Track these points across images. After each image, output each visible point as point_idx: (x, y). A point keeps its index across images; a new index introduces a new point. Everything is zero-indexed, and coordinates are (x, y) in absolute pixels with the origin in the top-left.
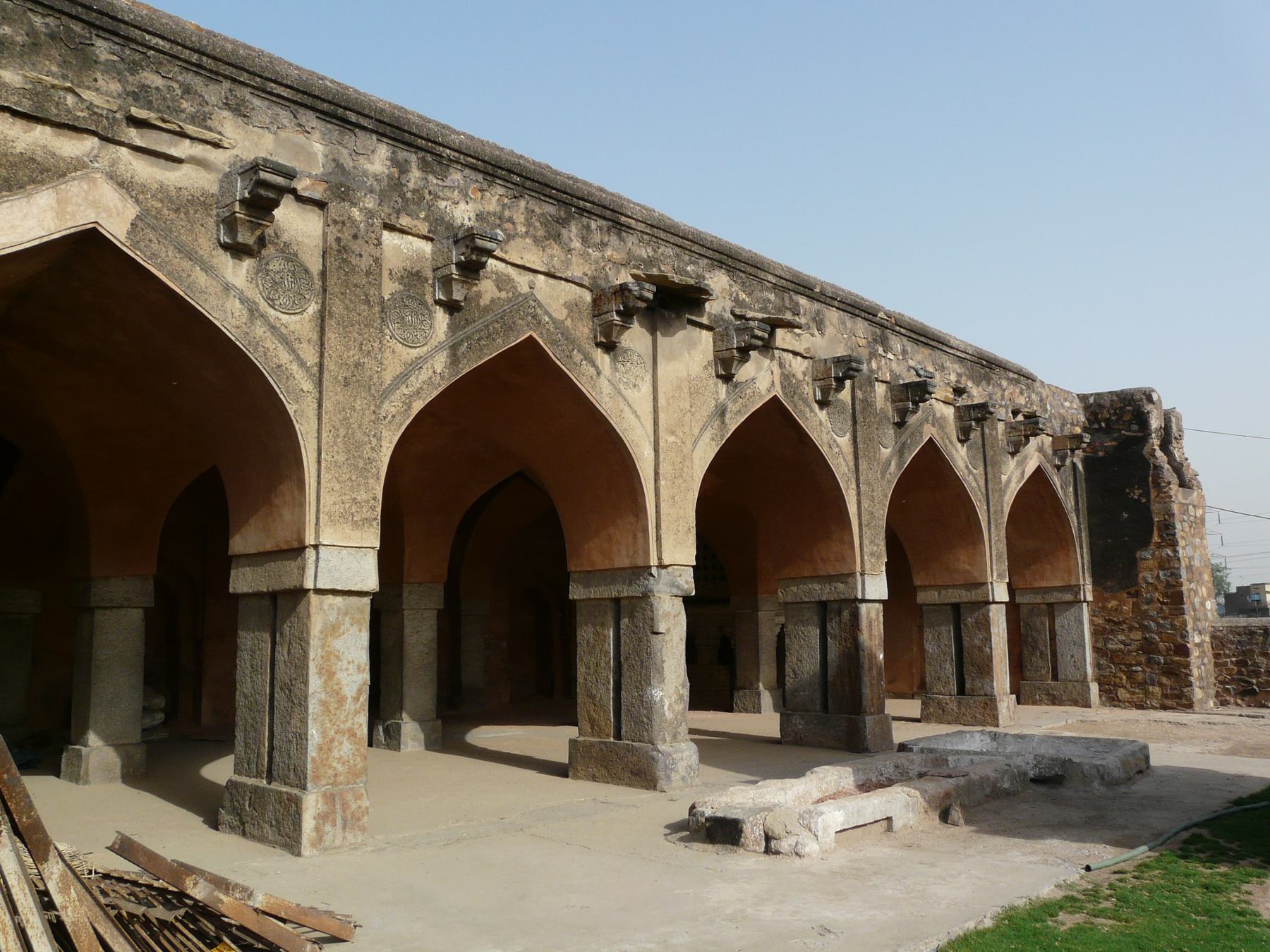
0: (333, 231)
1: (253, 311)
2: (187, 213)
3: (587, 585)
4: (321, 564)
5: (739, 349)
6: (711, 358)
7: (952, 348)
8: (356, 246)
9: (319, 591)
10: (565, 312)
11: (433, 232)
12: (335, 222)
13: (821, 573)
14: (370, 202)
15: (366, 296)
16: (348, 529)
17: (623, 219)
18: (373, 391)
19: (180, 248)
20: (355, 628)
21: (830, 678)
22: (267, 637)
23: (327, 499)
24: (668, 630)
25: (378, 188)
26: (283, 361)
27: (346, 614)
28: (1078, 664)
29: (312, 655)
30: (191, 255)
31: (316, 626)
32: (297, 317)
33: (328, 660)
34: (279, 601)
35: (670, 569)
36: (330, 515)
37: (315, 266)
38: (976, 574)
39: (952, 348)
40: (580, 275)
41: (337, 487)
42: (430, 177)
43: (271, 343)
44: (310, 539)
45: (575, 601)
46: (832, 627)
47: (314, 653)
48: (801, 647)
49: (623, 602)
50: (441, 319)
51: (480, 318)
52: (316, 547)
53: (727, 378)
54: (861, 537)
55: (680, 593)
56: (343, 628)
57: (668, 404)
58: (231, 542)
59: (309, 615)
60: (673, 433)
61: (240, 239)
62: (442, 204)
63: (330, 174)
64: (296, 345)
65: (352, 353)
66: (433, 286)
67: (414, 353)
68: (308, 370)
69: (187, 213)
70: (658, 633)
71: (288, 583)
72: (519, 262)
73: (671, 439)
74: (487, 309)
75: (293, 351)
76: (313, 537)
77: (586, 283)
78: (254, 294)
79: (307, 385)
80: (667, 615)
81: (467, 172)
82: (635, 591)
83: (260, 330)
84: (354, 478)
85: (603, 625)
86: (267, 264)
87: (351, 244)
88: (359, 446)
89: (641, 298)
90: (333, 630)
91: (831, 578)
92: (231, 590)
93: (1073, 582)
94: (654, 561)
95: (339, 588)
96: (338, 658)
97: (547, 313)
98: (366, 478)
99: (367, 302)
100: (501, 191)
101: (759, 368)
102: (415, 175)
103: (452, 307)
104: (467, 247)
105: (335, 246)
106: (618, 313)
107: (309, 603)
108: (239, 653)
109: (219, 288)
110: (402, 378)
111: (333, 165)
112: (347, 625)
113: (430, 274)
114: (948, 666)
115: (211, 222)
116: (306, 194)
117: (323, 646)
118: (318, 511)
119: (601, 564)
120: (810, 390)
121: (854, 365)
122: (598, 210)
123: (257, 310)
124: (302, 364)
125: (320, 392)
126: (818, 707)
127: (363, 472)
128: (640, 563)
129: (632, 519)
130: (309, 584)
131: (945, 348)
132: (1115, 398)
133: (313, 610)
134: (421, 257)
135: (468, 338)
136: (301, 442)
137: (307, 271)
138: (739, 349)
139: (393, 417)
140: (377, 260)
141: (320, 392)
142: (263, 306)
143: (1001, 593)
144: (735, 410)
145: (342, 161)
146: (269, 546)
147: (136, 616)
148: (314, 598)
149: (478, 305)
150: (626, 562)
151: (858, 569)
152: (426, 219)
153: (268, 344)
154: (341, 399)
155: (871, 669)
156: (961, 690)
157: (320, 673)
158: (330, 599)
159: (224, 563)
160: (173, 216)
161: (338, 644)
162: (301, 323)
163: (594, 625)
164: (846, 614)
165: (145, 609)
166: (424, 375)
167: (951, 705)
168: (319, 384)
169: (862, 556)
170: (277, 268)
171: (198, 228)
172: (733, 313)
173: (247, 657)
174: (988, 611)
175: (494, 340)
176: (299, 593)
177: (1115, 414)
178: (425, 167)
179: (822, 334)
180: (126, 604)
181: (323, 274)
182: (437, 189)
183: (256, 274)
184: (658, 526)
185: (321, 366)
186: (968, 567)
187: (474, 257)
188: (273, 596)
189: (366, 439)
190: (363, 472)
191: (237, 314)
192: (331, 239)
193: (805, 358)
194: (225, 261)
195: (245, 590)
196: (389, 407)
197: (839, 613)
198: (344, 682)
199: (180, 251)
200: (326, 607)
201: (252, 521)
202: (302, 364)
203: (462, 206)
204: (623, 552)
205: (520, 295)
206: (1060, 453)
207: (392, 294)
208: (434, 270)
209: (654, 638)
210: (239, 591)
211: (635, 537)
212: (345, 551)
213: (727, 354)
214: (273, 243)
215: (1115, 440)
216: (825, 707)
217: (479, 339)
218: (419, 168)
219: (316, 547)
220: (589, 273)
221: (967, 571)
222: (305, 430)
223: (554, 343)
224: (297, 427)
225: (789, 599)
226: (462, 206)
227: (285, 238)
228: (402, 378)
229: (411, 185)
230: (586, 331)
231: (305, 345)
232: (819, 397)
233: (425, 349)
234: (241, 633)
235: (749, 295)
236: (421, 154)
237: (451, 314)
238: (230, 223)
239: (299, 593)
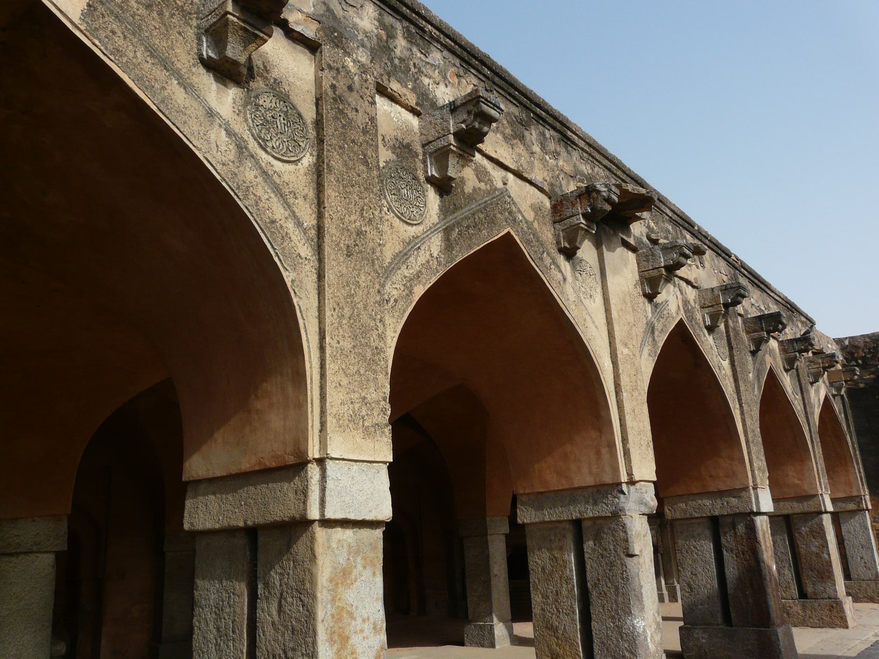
0: (328, 78)
1: (241, 148)
2: (161, 14)
3: (540, 508)
4: (330, 484)
5: (666, 267)
6: (638, 278)
7: (772, 291)
8: (352, 98)
9: (327, 523)
10: (532, 214)
11: (421, 106)
12: (330, 68)
13: (711, 489)
14: (363, 57)
15: (365, 156)
16: (358, 436)
17: (569, 133)
18: (377, 267)
19: (152, 52)
20: (367, 573)
21: (730, 591)
22: (242, 588)
23: (334, 397)
24: (641, 551)
25: (368, 45)
26: (277, 217)
27: (357, 552)
28: (869, 565)
29: (320, 614)
30: (166, 65)
31: (324, 572)
32: (291, 167)
33: (340, 620)
34: (261, 539)
35: (638, 485)
36: (338, 417)
37: (309, 114)
38: (806, 487)
39: (772, 291)
40: (541, 180)
41: (345, 382)
42: (415, 49)
43: (262, 191)
44: (314, 452)
45: (523, 525)
46: (727, 540)
47: (323, 612)
48: (694, 561)
49: (585, 524)
50: (432, 197)
51: (466, 206)
52: (321, 462)
53: (650, 297)
54: (749, 453)
55: (647, 511)
56: (355, 572)
57: (619, 316)
58: (186, 465)
59: (313, 557)
60: (626, 345)
61: (230, 53)
62: (426, 81)
63: (322, 16)
64: (291, 201)
65: (353, 218)
66: (424, 162)
67: (412, 231)
68: (305, 231)
69: (161, 14)
70: (632, 556)
71: (280, 512)
72: (494, 155)
73: (626, 351)
74: (470, 198)
75: (287, 205)
76: (317, 448)
77: (546, 188)
78: (240, 128)
79: (305, 251)
80: (638, 535)
81: (446, 53)
82: (603, 510)
83: (249, 174)
84: (362, 372)
85: (561, 549)
86: (257, 97)
87: (347, 94)
88: (365, 331)
89: (608, 200)
90: (343, 576)
91: (721, 494)
92: (186, 526)
93: (855, 493)
94: (624, 478)
95: (352, 517)
96: (351, 615)
97: (520, 211)
98: (375, 372)
99: (366, 163)
100: (475, 81)
101: (668, 292)
102: (401, 44)
103: (443, 186)
104: (469, 113)
105: (330, 92)
106: (585, 216)
107: (313, 539)
108: (197, 611)
109: (201, 112)
110: (402, 257)
111: (324, 8)
112: (360, 568)
113: (420, 150)
114: (787, 572)
115: (191, 33)
116: (298, 29)
117: (333, 600)
118: (323, 412)
119: (555, 482)
120: (701, 317)
121: (742, 291)
122: (550, 120)
123: (246, 148)
124: (299, 224)
125: (321, 261)
126: (720, 620)
127: (371, 364)
128: (608, 479)
129: (594, 434)
130: (314, 513)
131: (768, 291)
132: (868, 340)
133: (319, 549)
134: (409, 131)
135: (459, 224)
136: (301, 321)
137: (300, 116)
138: (666, 267)
139: (396, 301)
140: (373, 119)
141: (321, 261)
142: (253, 145)
143: (766, 502)
144: (660, 329)
145: (332, 7)
146: (246, 464)
147: (45, 562)
148: (320, 533)
149: (463, 191)
150: (589, 481)
151: (751, 484)
152: (414, 90)
153: (260, 192)
154: (344, 271)
155: (771, 581)
156: (803, 595)
157: (331, 641)
158: (339, 533)
159: (172, 491)
160: (142, 11)
161: (350, 596)
162: (296, 174)
163: (550, 550)
164: (741, 528)
165: (58, 554)
166: (423, 257)
167: (795, 608)
168: (319, 250)
169: (753, 471)
170: (268, 105)
171: (174, 36)
172: (649, 238)
173: (211, 617)
174: (821, 520)
175: (480, 230)
176: (301, 525)
177: (870, 352)
178: (409, 37)
179: (703, 267)
180: (35, 548)
181: (319, 123)
182: (421, 64)
183: (245, 106)
184: (625, 440)
185: (320, 229)
186: (797, 482)
187: (477, 125)
188: (252, 533)
189: (372, 324)
190: (371, 364)
191: (223, 148)
192: (326, 84)
193: (693, 287)
194: (206, 81)
195: (209, 525)
196: (393, 289)
197: (734, 527)
198: (359, 650)
199: (152, 56)
200: (334, 545)
201: (219, 435)
202: (299, 224)
203: (442, 87)
204: (585, 470)
205: (496, 189)
206: (837, 384)
207: (386, 162)
208: (423, 146)
209: (628, 561)
210: (199, 526)
211: (598, 453)
212: (355, 467)
213: (655, 273)
214: (261, 76)
215: (872, 373)
216: (727, 619)
217: (468, 227)
218: (405, 38)
219: (321, 462)
220: (548, 179)
221: (797, 485)
222: (305, 303)
223: (528, 242)
224: (295, 300)
225: (678, 515)
226: (442, 87)
227: (275, 74)
228: (402, 257)
229: (398, 52)
230: (550, 236)
231: (300, 201)
232: (708, 322)
233: (420, 228)
234: (199, 582)
235: (656, 223)
236: (406, 24)
237: (441, 196)
238: (217, 33)
239: (301, 525)
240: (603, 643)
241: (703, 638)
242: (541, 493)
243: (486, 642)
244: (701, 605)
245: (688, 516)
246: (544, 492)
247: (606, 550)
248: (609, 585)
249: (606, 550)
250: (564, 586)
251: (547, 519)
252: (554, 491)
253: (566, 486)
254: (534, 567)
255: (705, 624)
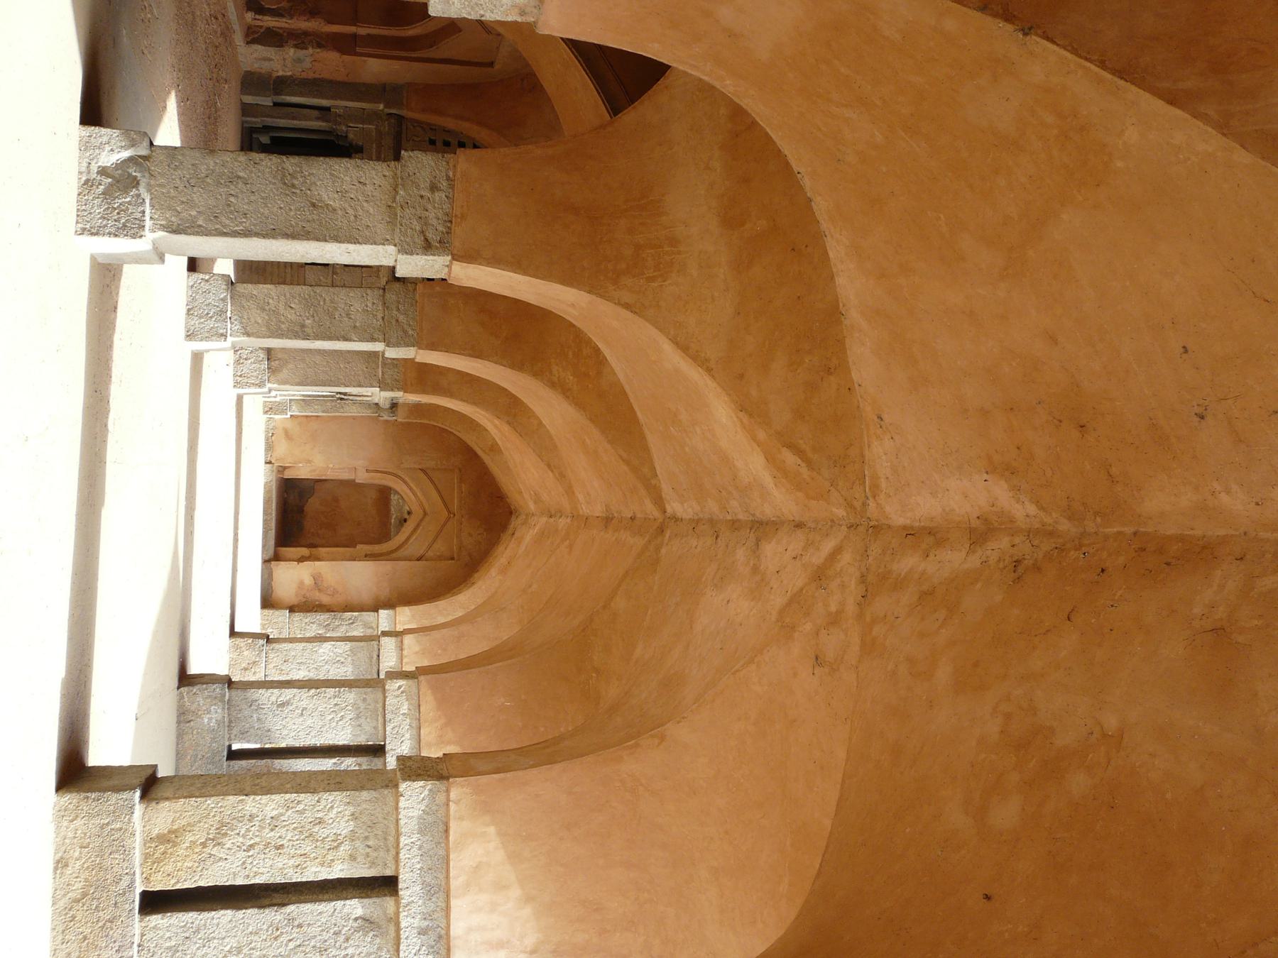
49: (389, 902)
85: (353, 858)
119: (461, 862)
129: (530, 941)
163: (352, 836)
240: (198, 931)
241: (210, 719)
242: (447, 831)
243: (195, 321)
244: (259, 719)
245: (388, 716)
246: (447, 837)
247: (347, 940)
248: (291, 945)
249: (347, 940)
250: (291, 862)
251: (404, 840)
252: (448, 856)
253: (455, 884)
254: (323, 802)
255: (230, 722)
